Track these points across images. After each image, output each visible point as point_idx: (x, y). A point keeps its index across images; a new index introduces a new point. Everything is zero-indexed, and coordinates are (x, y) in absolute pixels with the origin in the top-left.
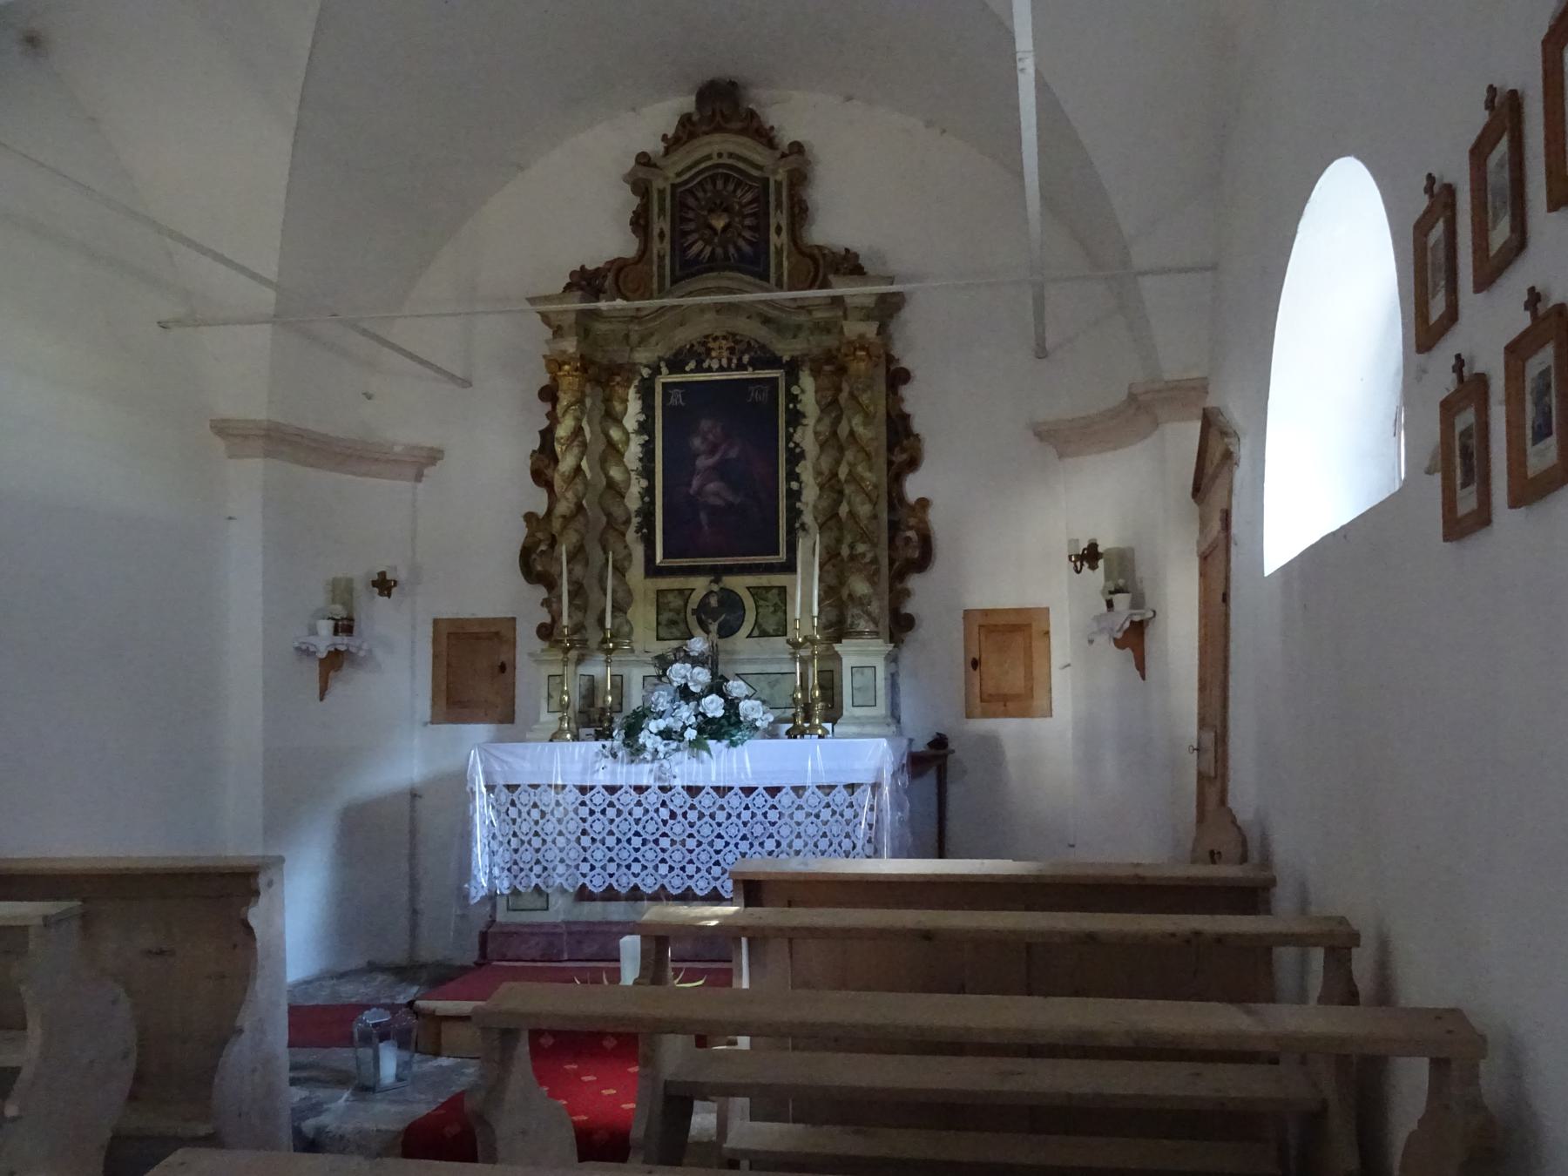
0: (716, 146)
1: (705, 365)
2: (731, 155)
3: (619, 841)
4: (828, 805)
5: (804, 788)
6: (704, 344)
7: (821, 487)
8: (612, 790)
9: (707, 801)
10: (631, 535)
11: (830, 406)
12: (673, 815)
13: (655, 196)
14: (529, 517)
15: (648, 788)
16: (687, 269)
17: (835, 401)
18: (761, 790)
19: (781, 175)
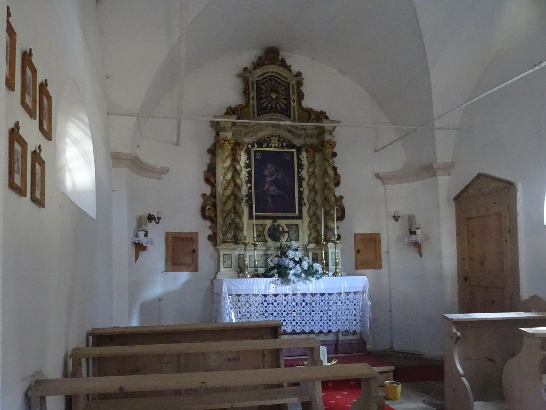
0: (272, 69)
1: (270, 145)
2: (276, 73)
3: (278, 314)
4: (348, 299)
5: (341, 293)
6: (269, 138)
7: (310, 190)
8: (275, 295)
9: (299, 299)
10: (244, 204)
11: (312, 163)
12: (297, 304)
13: (250, 84)
14: (204, 195)
15: (288, 294)
16: (262, 111)
17: (314, 161)
18: (326, 294)
19: (294, 82)
